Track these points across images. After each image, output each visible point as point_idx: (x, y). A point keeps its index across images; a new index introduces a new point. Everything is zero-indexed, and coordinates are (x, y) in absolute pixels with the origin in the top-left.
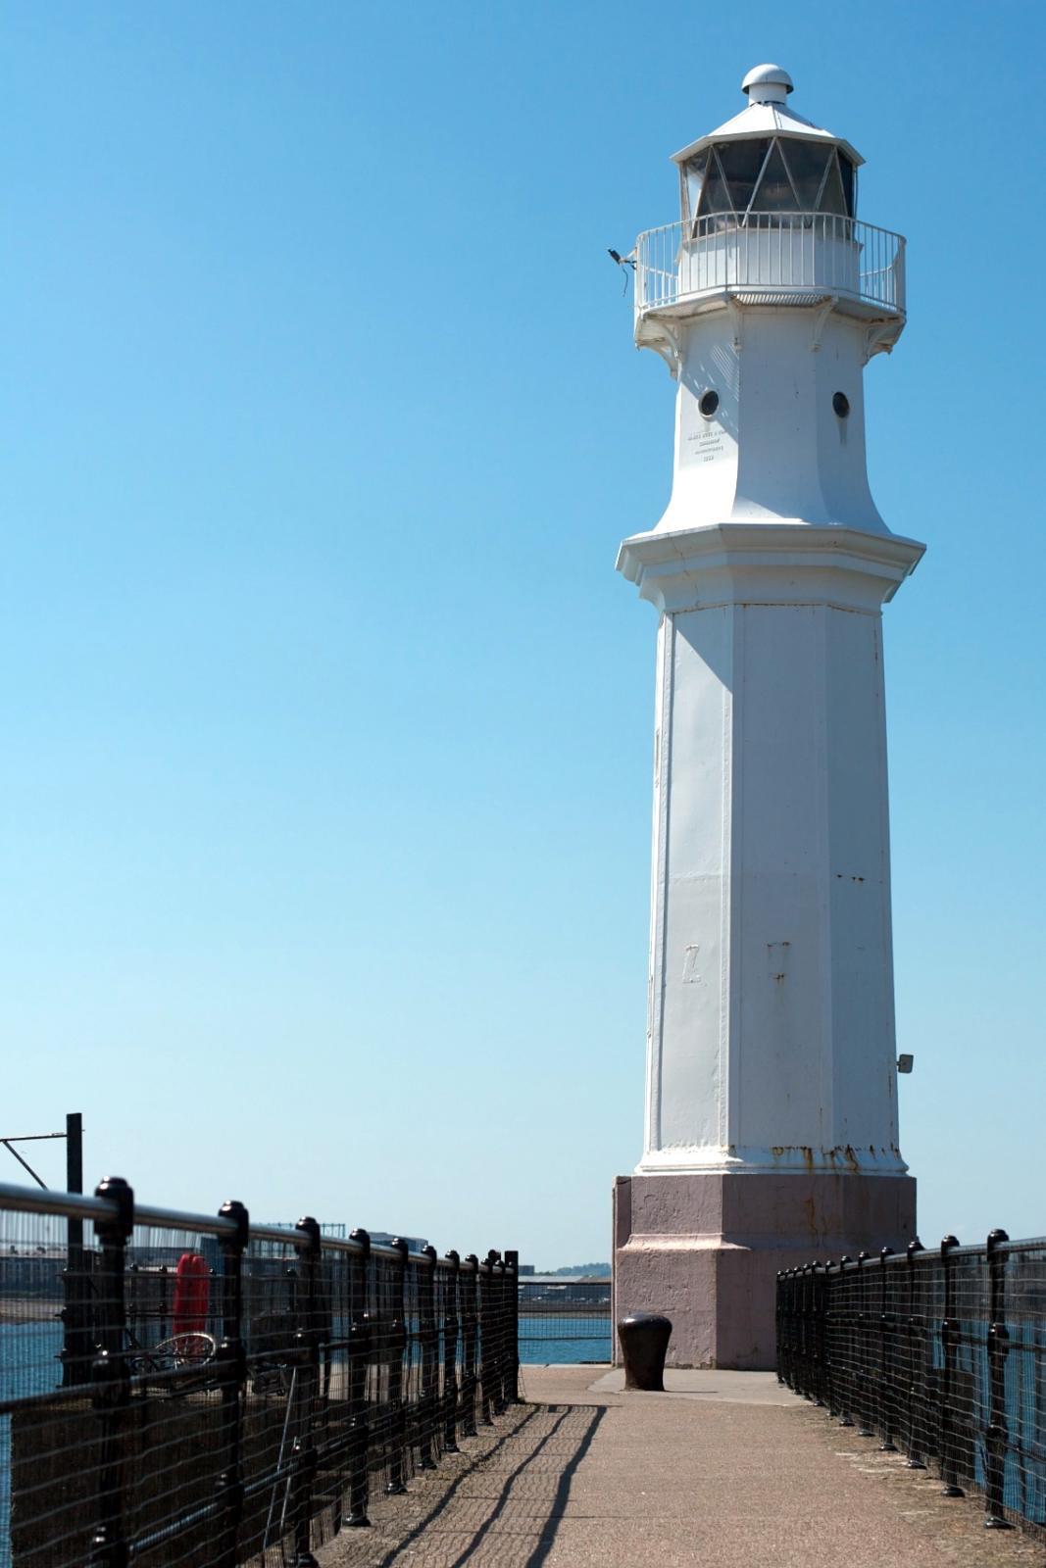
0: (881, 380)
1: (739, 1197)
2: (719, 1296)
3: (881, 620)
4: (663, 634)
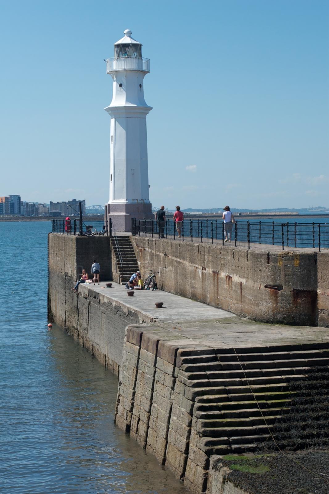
0: (147, 80)
1: (128, 207)
2: (125, 221)
4: (113, 121)
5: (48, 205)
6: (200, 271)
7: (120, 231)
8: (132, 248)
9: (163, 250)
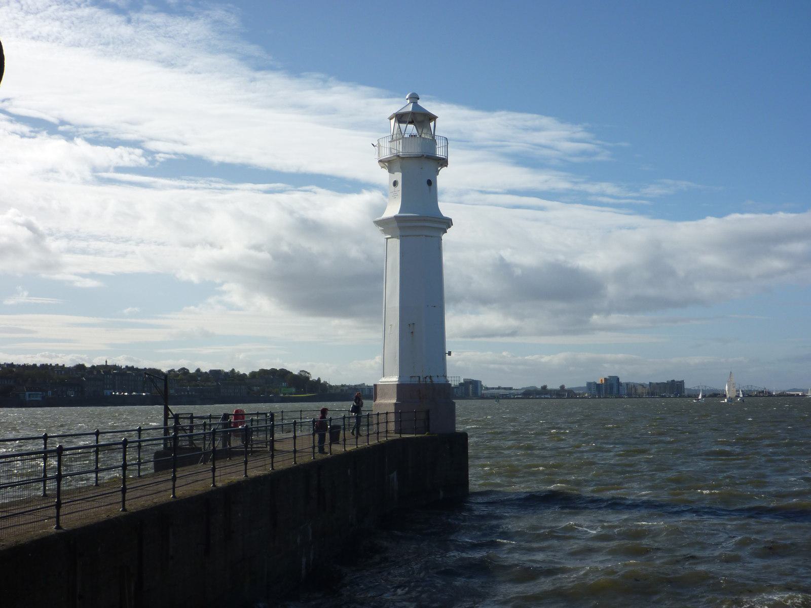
3: (253, 374)
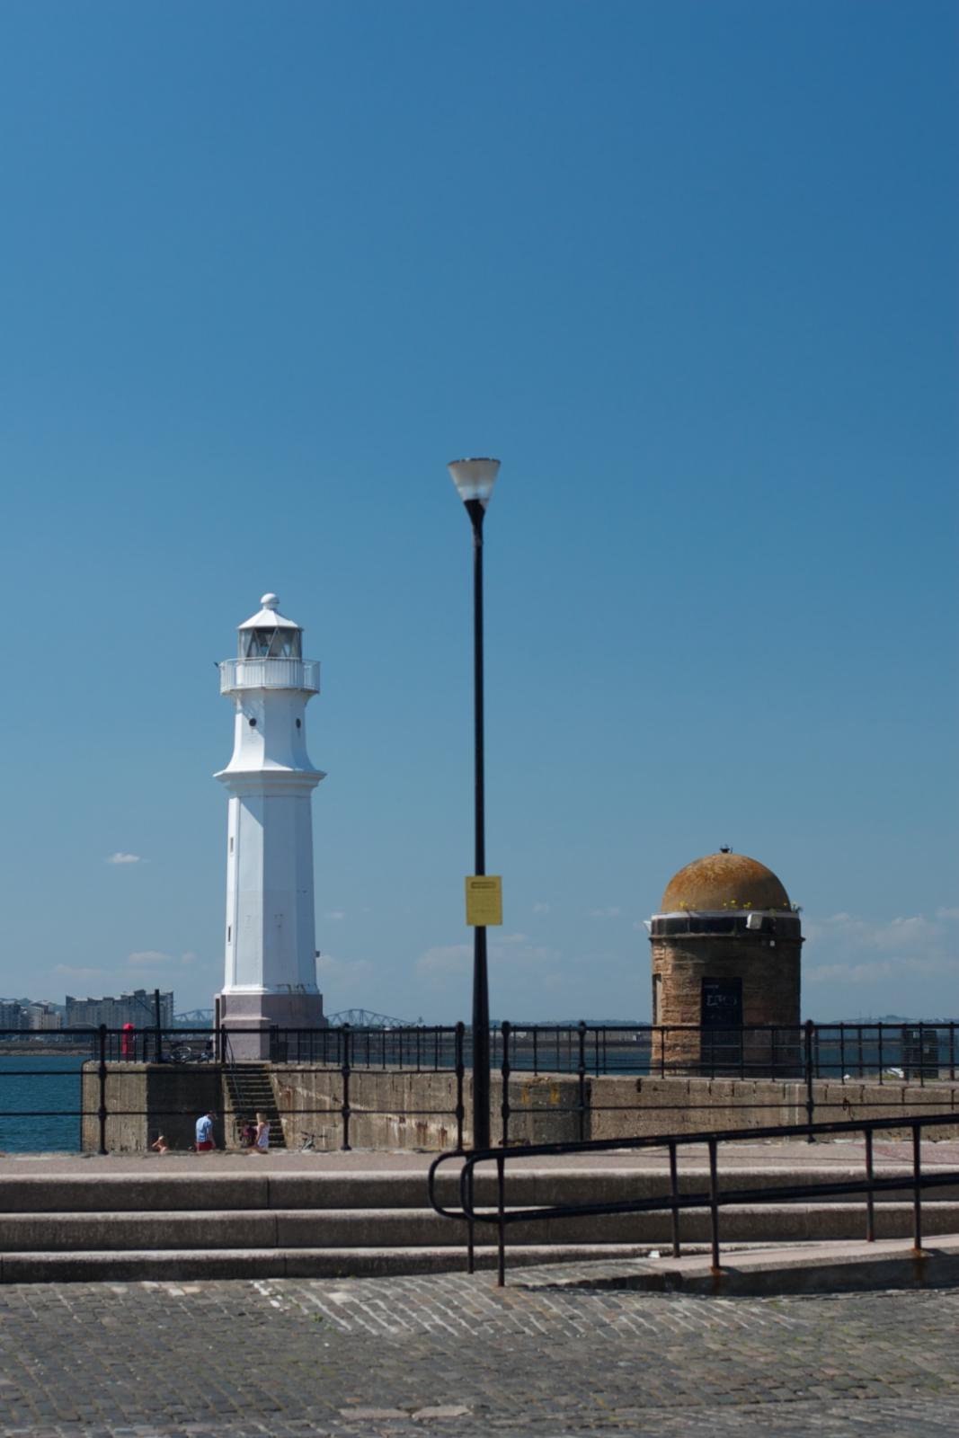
1: (267, 1002)
5: (59, 1008)
6: (395, 1126)
7: (247, 1051)
8: (271, 1090)
9: (331, 1090)
